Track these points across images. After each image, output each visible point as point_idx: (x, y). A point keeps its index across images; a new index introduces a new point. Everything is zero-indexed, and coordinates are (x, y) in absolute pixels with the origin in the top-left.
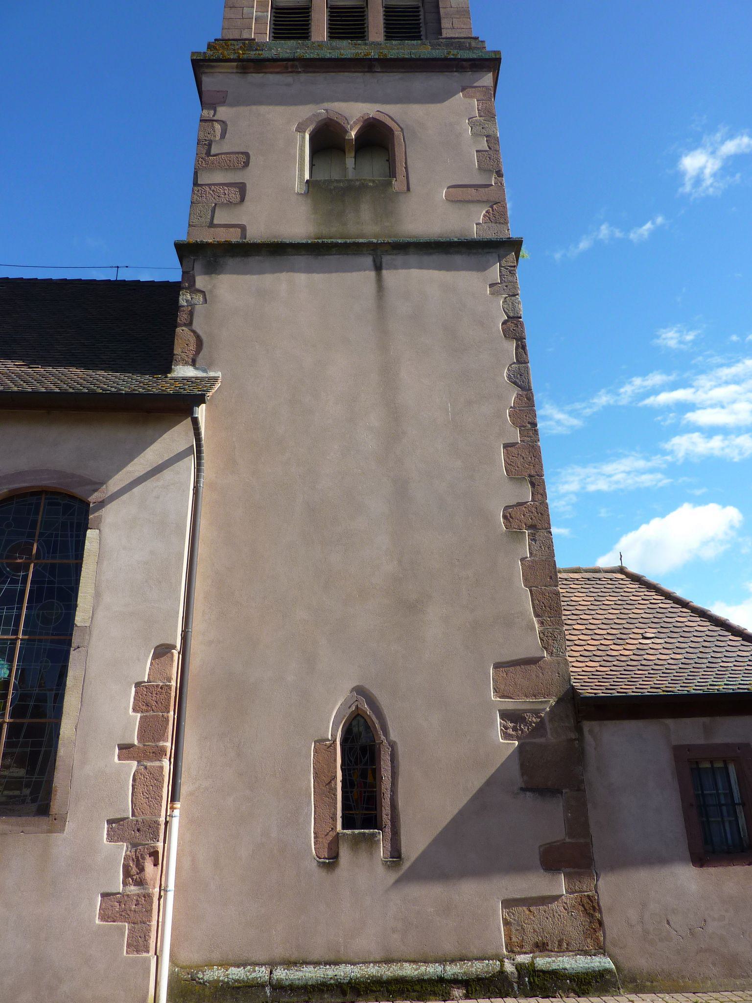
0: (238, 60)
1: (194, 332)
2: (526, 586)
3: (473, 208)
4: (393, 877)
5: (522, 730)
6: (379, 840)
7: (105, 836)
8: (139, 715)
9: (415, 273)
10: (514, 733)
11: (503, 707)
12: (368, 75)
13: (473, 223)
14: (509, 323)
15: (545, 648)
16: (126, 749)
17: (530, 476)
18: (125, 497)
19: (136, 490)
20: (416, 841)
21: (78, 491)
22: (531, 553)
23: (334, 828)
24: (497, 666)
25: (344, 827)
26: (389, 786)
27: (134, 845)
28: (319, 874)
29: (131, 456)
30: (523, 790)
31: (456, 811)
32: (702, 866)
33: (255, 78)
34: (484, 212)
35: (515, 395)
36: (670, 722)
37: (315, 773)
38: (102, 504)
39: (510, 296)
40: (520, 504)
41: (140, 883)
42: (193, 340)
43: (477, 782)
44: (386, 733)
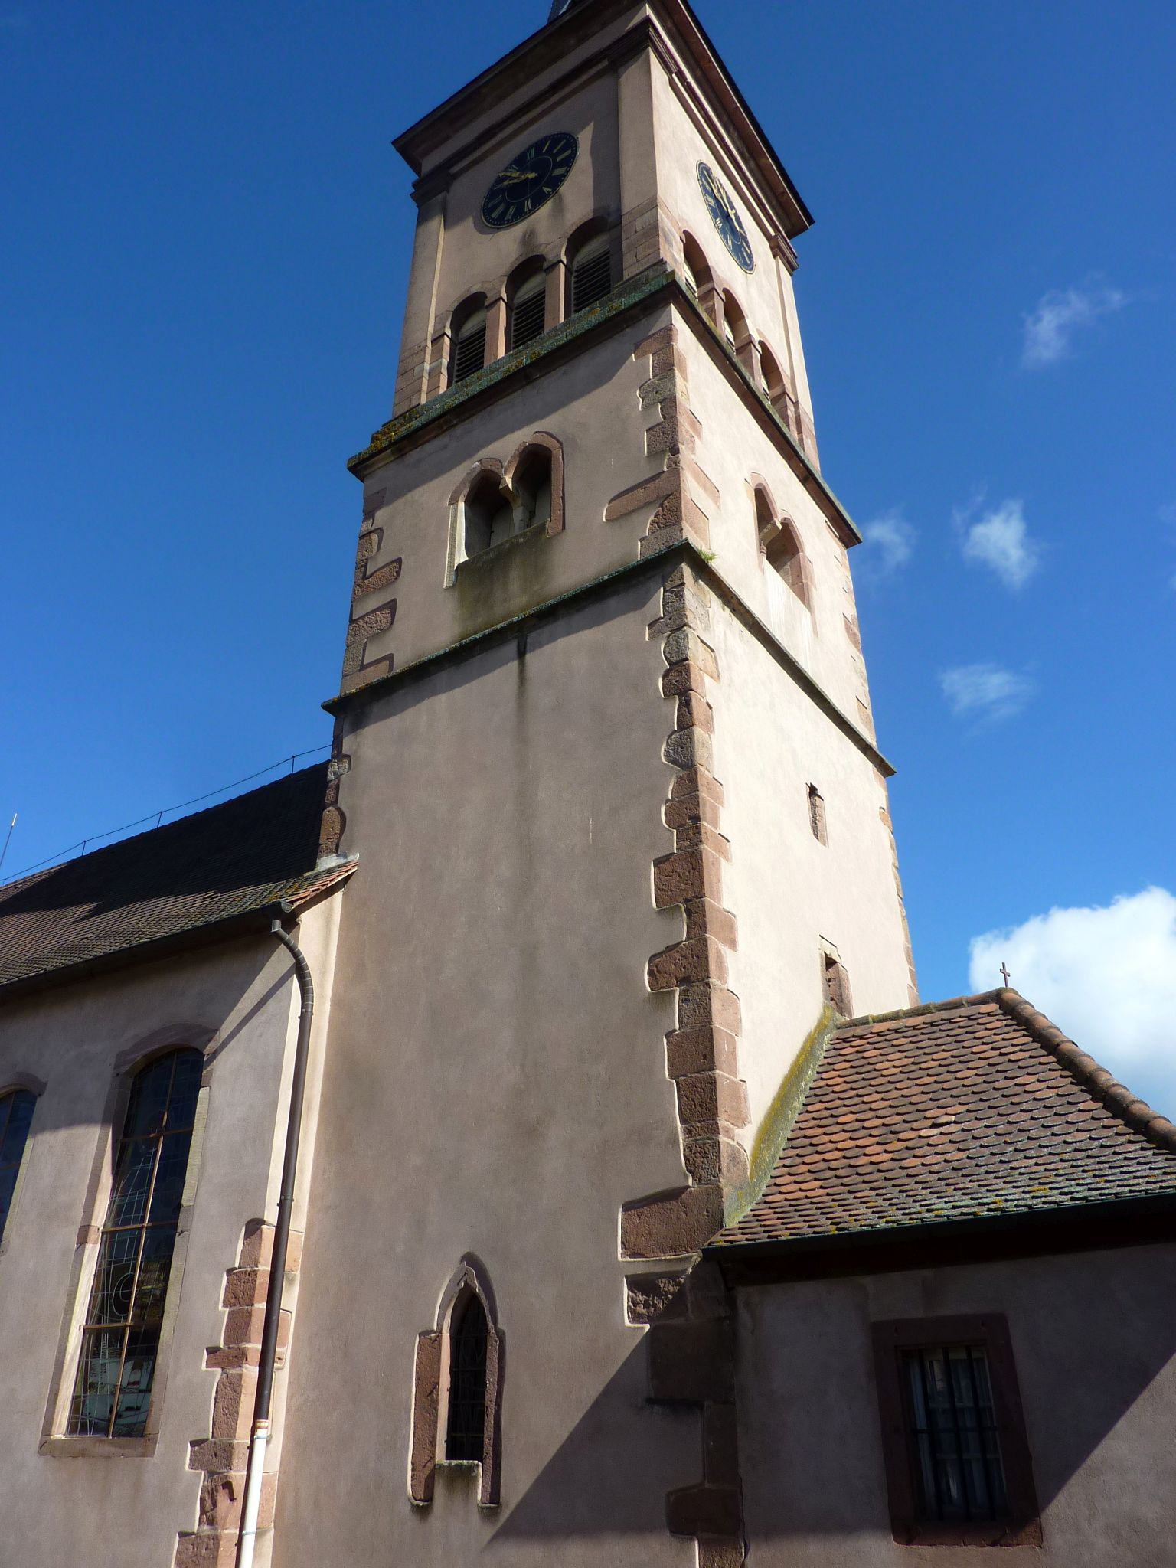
0: (391, 445)
1: (339, 809)
2: (671, 1076)
3: (636, 518)
4: (489, 1531)
5: (654, 1305)
6: (476, 1477)
7: (188, 1461)
8: (227, 1310)
9: (562, 643)
10: (644, 1311)
11: (632, 1271)
12: (528, 388)
13: (637, 544)
14: (672, 673)
15: (691, 1172)
16: (212, 1351)
17: (687, 901)
18: (232, 1043)
19: (243, 1031)
20: (518, 1481)
21: (196, 1044)
22: (680, 1023)
23: (432, 1458)
24: (628, 1207)
25: (450, 1455)
26: (493, 1397)
27: (211, 1474)
28: (411, 1520)
29: (242, 990)
30: (651, 1401)
31: (566, 1436)
32: (909, 1542)
33: (414, 455)
34: (652, 518)
35: (673, 780)
36: (867, 1281)
37: (418, 1379)
38: (214, 1055)
39: (674, 631)
40: (670, 948)
41: (212, 1522)
42: (337, 820)
43: (591, 1389)
44: (495, 1321)
